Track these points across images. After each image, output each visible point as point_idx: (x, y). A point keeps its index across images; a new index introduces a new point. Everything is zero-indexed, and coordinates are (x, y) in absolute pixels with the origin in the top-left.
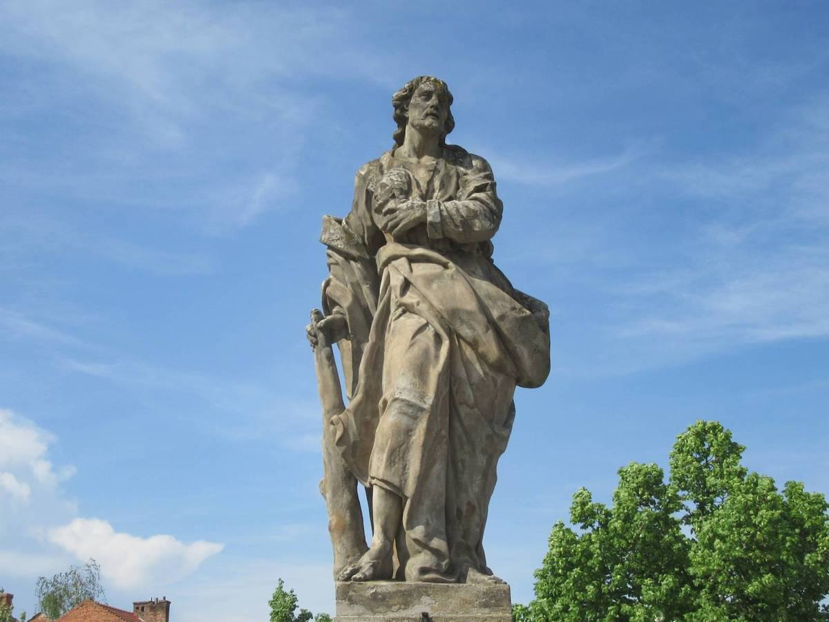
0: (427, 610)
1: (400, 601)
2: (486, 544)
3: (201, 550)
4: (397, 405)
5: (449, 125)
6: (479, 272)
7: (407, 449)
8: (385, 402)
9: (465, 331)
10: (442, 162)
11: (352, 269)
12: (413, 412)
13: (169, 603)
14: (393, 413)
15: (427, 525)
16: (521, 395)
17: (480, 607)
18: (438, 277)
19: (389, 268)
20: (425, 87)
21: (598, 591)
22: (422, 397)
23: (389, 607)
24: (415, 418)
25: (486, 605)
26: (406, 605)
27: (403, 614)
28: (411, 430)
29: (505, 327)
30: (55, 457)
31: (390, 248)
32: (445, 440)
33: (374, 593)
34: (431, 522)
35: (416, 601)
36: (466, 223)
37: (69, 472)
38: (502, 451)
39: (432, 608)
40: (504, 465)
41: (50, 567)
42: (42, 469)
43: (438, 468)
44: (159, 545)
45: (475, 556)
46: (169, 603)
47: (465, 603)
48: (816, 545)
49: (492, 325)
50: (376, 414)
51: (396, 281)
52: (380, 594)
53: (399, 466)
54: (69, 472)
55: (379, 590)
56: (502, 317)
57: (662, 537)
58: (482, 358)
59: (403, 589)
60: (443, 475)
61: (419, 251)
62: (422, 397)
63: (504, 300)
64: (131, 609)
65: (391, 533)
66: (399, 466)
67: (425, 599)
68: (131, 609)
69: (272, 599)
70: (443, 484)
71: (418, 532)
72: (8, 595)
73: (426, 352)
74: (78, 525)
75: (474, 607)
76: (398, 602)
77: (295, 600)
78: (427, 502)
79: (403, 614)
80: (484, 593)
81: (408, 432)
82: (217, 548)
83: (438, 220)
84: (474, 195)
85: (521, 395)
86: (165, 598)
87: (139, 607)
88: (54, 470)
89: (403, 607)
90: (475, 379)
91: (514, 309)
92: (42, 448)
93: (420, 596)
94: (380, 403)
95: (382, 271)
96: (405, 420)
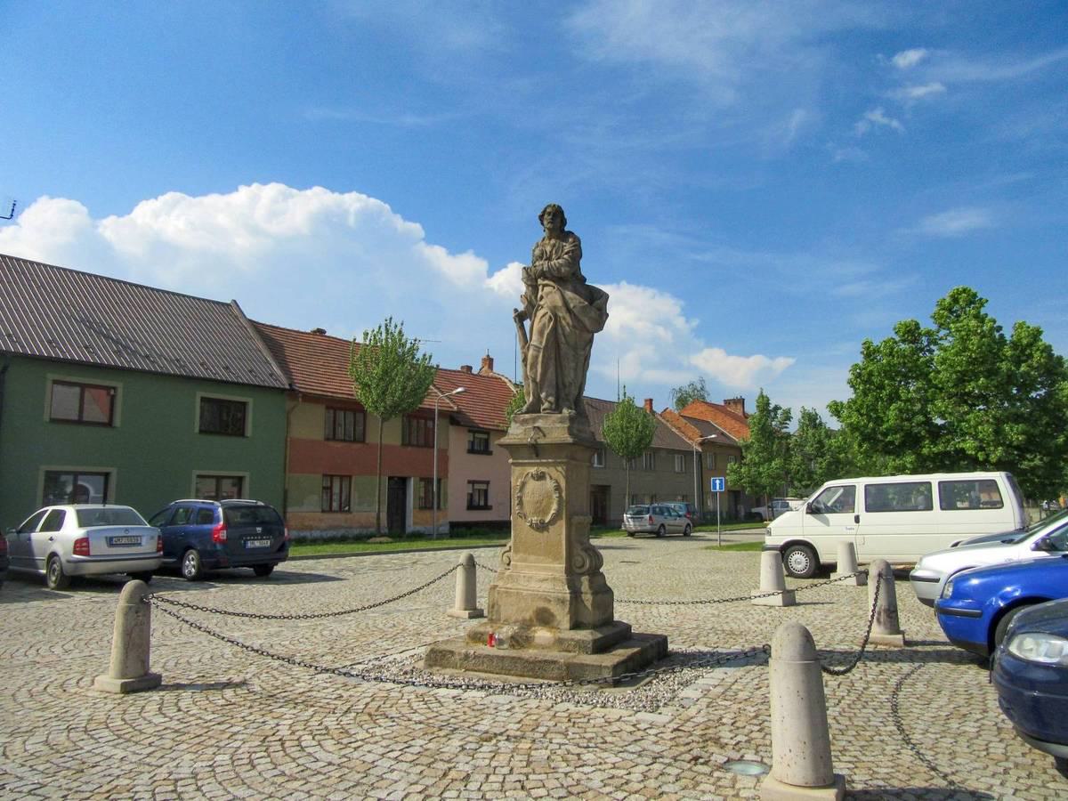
3: (782, 363)
5: (564, 222)
6: (570, 287)
7: (537, 364)
9: (560, 314)
10: (558, 241)
12: (537, 349)
13: (744, 399)
15: (547, 392)
18: (551, 292)
20: (548, 210)
22: (541, 343)
24: (539, 352)
29: (575, 311)
30: (687, 313)
36: (558, 269)
37: (695, 323)
41: (682, 380)
42: (680, 322)
43: (552, 370)
44: (757, 361)
46: (744, 399)
47: (554, 422)
49: (569, 310)
53: (534, 370)
54: (695, 323)
56: (574, 307)
57: (1011, 356)
58: (568, 324)
62: (541, 343)
63: (576, 299)
64: (723, 404)
66: (534, 370)
71: (543, 395)
73: (544, 325)
74: (706, 352)
77: (768, 400)
78: (547, 383)
81: (537, 357)
82: (791, 361)
87: (727, 402)
88: (687, 322)
90: (566, 333)
91: (580, 303)
92: (678, 310)
96: (535, 353)
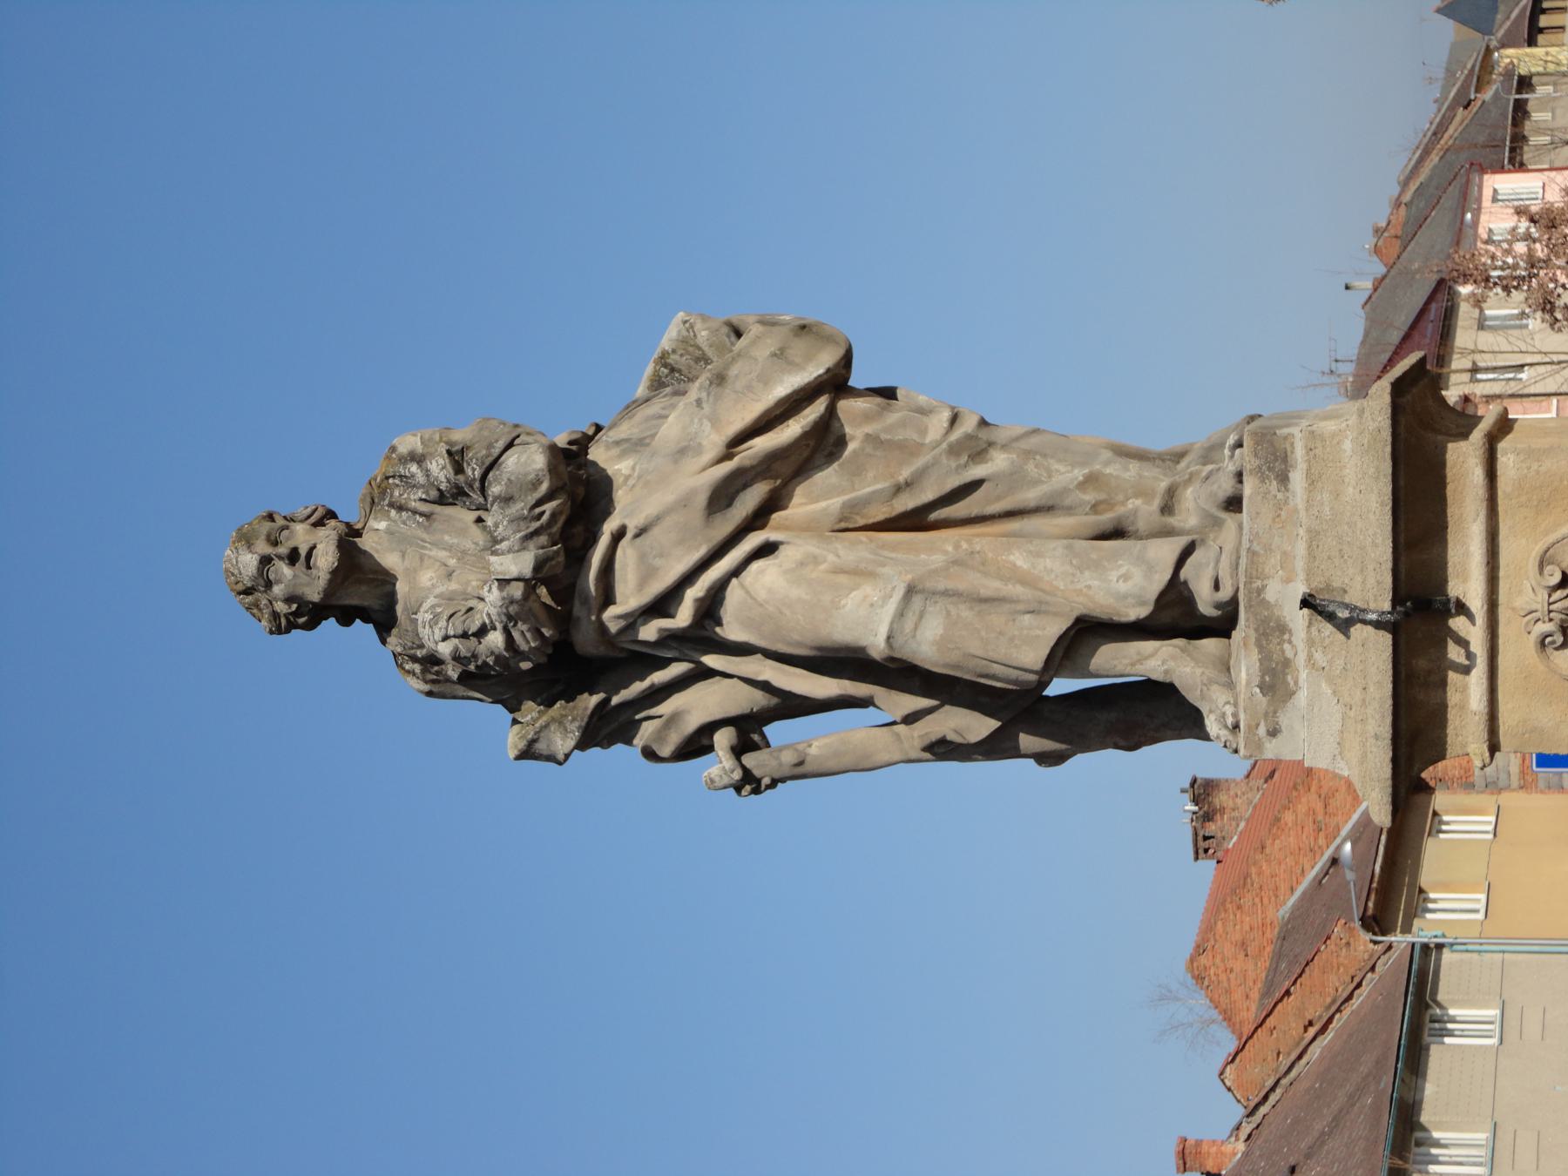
1: (1275, 641)
13: (1194, 781)
17: (1287, 490)
21: (1403, 1153)
23: (1287, 663)
25: (1284, 479)
26: (1282, 629)
28: (869, 503)
33: (1261, 688)
34: (1123, 570)
48: (1279, 491)
52: (1262, 677)
68: (1208, 866)
72: (1197, 1141)
75: (1286, 502)
76: (1279, 644)
86: (1183, 791)
89: (1286, 637)
95: (623, 649)
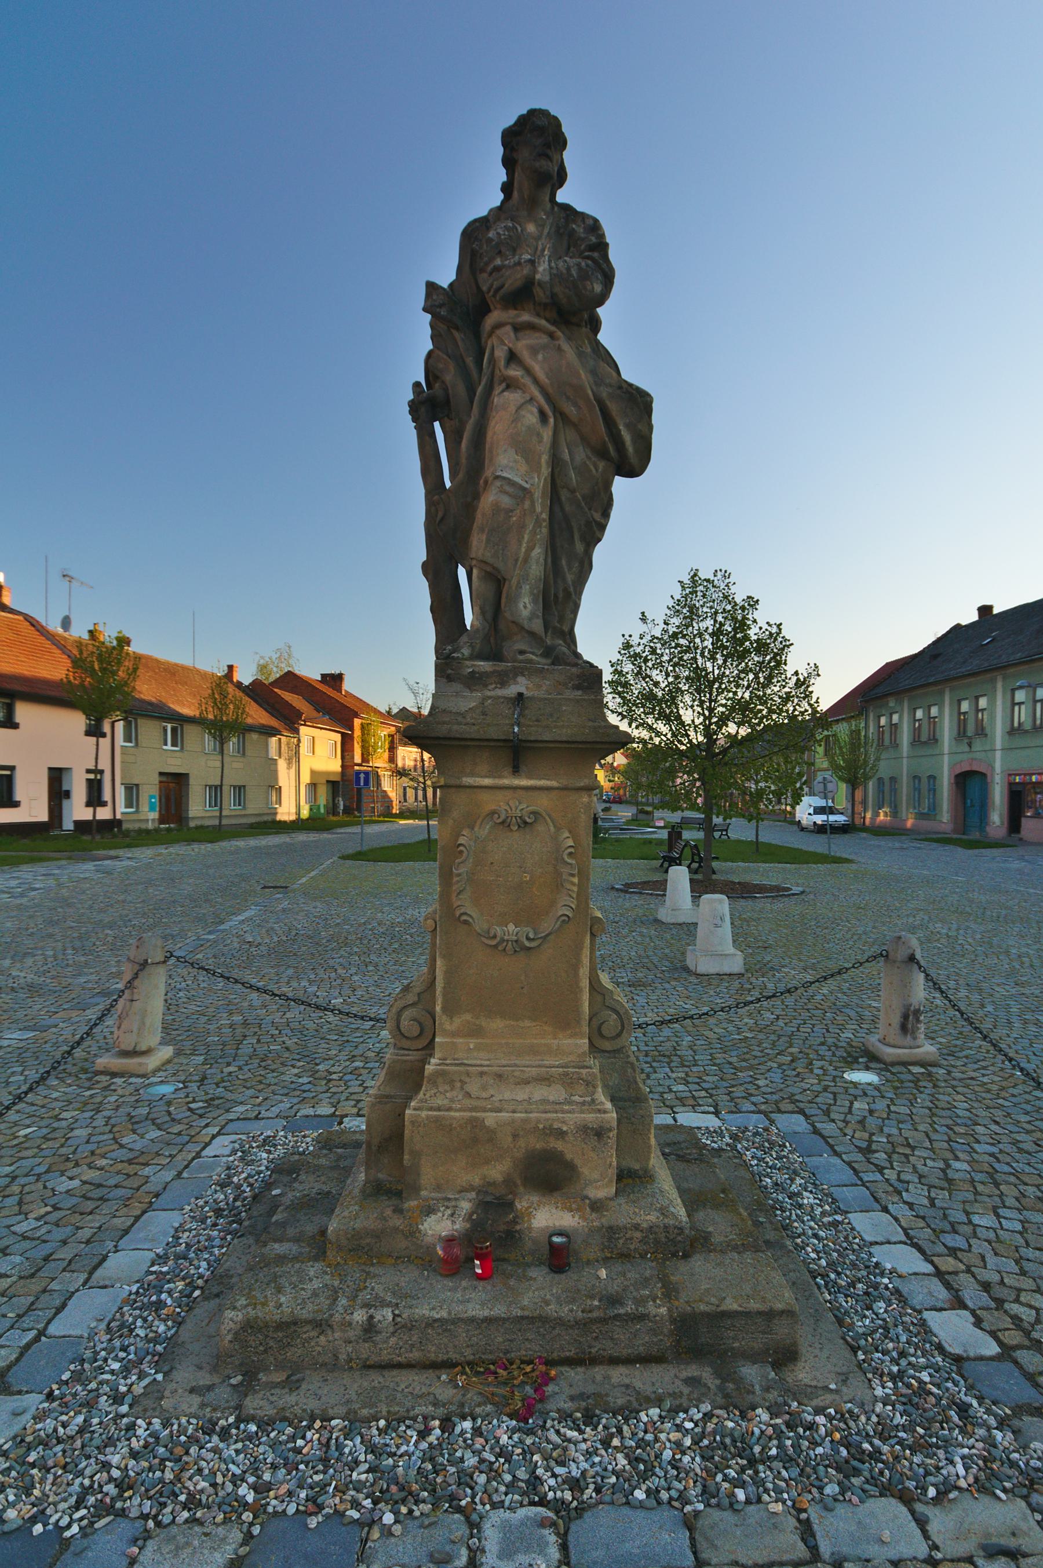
0: (523, 690)
2: (579, 630)
4: (498, 483)
8: (486, 482)
11: (455, 339)
14: (494, 492)
16: (620, 485)
19: (494, 340)
23: (486, 686)
25: (577, 687)
26: (503, 684)
27: (499, 692)
31: (495, 316)
32: (544, 524)
34: (528, 605)
35: (511, 682)
38: (599, 540)
39: (527, 688)
40: (599, 553)
45: (569, 641)
50: (477, 496)
51: (500, 354)
55: (477, 669)
59: (499, 669)
60: (542, 560)
61: (526, 317)
65: (489, 616)
67: (520, 679)
69: (245, 676)
70: (542, 568)
79: (499, 692)
80: (578, 676)
83: (547, 278)
84: (587, 254)
85: (620, 485)
93: (516, 675)
94: (482, 482)
